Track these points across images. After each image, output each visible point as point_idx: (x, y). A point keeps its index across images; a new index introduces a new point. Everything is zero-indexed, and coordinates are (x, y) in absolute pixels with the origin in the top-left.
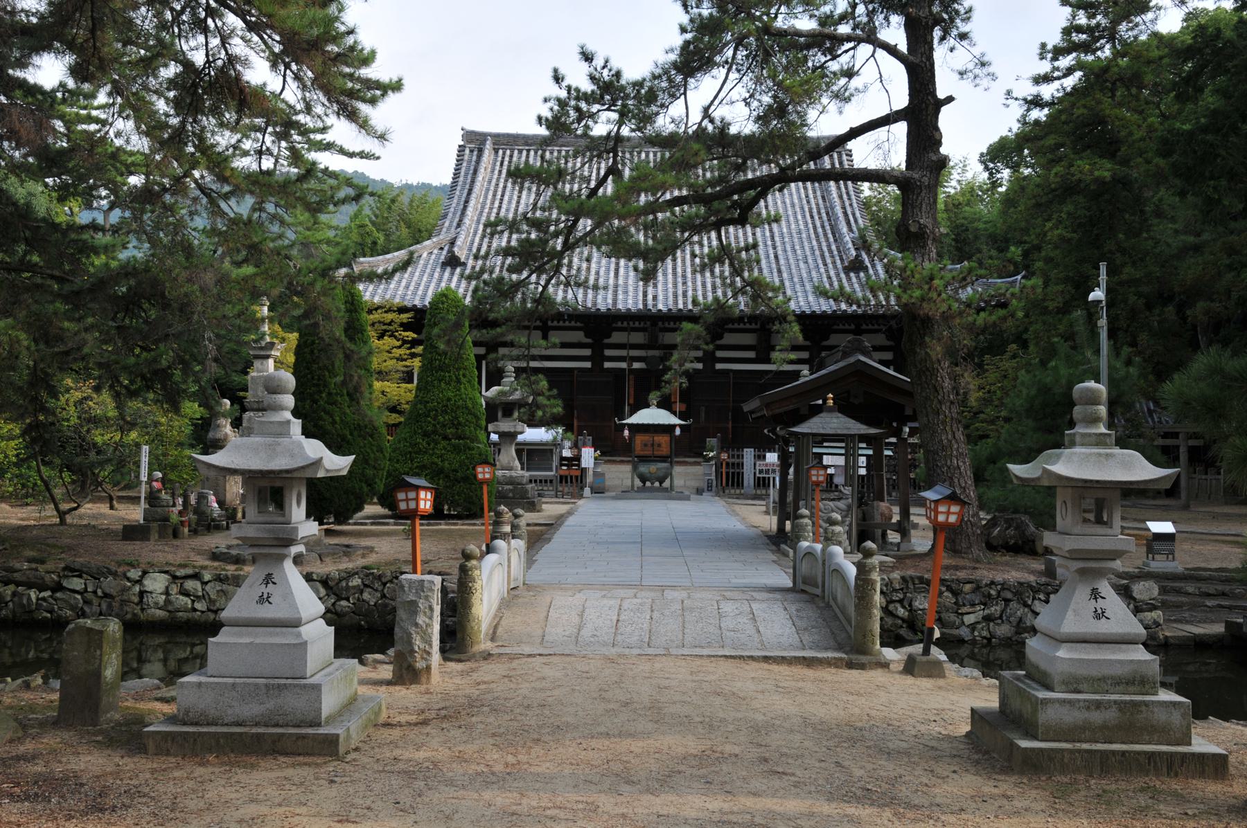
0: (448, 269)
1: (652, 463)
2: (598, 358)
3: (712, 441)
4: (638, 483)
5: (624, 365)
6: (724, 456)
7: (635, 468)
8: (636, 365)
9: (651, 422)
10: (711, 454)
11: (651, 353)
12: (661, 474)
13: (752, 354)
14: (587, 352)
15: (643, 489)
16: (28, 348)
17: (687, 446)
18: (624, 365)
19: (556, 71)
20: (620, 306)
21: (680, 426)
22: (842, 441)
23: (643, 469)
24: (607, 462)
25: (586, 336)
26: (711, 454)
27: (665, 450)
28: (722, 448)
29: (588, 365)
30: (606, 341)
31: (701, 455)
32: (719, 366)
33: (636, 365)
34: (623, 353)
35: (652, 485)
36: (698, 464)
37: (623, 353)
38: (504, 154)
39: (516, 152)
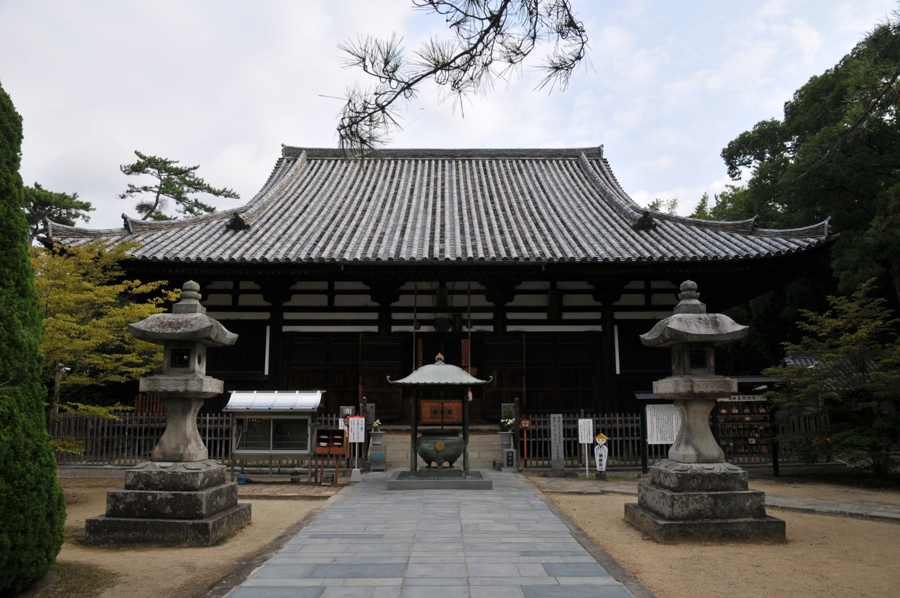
0: (231, 232)
1: (437, 441)
2: (385, 322)
3: (507, 407)
4: (421, 463)
5: (411, 329)
6: (526, 424)
7: (415, 442)
8: (424, 329)
9: (436, 381)
10: (510, 422)
11: (439, 315)
12: (450, 451)
13: (543, 316)
14: (374, 316)
15: (428, 473)
16: (533, 423)
17: (480, 409)
18: (411, 329)
20: (403, 255)
21: (473, 387)
23: (426, 445)
24: (388, 432)
25: (373, 300)
26: (510, 422)
27: (457, 416)
28: (521, 414)
29: (375, 329)
30: (394, 304)
31: (496, 421)
32: (510, 328)
33: (424, 329)
35: (439, 467)
36: (495, 432)
39: (460, 162)
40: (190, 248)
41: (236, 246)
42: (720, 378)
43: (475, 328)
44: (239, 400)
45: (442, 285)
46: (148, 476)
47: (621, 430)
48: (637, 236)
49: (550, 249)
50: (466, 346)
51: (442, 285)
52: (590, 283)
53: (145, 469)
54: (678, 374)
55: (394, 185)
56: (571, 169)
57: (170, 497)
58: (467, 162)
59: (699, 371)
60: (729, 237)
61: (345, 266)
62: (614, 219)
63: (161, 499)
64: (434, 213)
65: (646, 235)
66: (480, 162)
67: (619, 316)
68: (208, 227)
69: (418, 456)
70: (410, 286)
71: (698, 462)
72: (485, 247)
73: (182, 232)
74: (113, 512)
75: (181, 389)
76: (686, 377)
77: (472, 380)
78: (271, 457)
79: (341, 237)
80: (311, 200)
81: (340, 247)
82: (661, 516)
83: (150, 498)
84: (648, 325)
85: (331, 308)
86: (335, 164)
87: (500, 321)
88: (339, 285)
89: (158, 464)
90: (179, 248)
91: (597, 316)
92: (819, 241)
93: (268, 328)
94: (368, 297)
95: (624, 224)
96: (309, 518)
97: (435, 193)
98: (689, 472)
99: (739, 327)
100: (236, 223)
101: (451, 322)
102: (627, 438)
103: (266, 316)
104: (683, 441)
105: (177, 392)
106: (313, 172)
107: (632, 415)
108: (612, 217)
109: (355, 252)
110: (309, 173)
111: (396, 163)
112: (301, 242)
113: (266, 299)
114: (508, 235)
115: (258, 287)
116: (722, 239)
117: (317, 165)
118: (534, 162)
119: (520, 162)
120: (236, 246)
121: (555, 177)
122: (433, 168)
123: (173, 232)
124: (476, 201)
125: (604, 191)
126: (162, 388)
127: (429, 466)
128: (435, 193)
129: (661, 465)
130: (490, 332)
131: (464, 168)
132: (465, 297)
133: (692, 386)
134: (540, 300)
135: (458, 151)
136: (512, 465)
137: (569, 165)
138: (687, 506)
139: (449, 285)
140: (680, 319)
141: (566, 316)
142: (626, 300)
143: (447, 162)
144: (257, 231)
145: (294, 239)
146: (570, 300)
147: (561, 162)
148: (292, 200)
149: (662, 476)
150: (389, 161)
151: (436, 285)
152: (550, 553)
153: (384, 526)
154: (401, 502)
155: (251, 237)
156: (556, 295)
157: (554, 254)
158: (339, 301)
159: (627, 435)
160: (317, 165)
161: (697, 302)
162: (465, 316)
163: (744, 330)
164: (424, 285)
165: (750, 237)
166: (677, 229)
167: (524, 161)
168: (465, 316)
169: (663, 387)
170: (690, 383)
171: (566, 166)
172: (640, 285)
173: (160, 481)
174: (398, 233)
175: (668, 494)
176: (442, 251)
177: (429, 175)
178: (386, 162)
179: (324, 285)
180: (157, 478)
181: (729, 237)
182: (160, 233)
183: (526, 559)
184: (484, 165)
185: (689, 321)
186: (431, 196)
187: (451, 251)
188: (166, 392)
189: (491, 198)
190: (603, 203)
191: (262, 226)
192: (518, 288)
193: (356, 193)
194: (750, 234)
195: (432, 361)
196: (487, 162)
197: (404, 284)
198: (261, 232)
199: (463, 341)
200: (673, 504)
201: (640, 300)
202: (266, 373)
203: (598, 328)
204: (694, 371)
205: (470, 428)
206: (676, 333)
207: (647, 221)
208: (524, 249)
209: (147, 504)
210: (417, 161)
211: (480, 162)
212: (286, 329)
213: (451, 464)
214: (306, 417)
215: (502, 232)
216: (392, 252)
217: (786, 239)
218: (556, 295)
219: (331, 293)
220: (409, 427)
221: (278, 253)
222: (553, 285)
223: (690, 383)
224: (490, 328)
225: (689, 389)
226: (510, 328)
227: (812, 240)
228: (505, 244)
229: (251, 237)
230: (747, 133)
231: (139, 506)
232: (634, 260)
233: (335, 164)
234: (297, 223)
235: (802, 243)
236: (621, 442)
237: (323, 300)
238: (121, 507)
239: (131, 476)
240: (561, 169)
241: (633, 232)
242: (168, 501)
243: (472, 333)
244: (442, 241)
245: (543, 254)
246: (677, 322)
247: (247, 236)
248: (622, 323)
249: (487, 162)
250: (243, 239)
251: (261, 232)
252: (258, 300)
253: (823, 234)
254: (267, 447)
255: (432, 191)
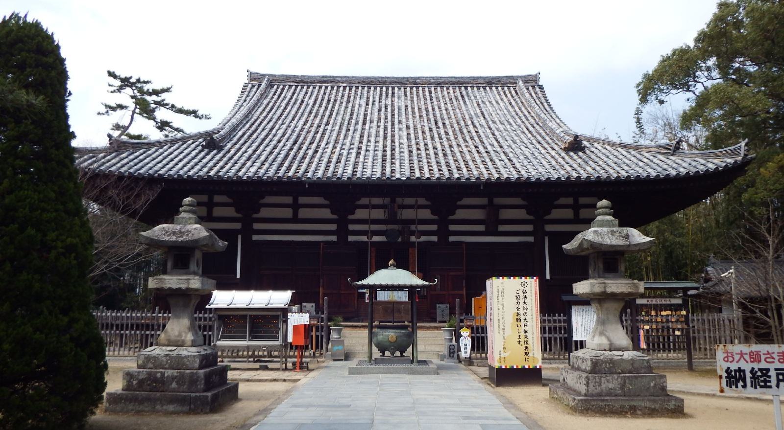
2: (343, 232)
4: (377, 354)
5: (364, 238)
8: (376, 238)
11: (390, 227)
13: (481, 228)
14: (333, 227)
17: (422, 308)
18: (364, 238)
19: (109, 72)
22: (286, 194)
29: (334, 238)
30: (350, 217)
32: (452, 239)
33: (376, 238)
34: (364, 227)
35: (398, 352)
37: (364, 227)
38: (278, 88)
39: (408, 89)
40: (170, 165)
41: (211, 164)
42: (630, 281)
43: (423, 239)
44: (222, 299)
45: (393, 201)
46: (155, 358)
47: (550, 328)
48: (567, 158)
49: (488, 170)
50: (414, 254)
51: (393, 201)
52: (523, 199)
53: (153, 352)
54: (594, 278)
55: (349, 110)
56: (509, 95)
57: (175, 374)
58: (415, 89)
59: (611, 275)
60: (651, 158)
61: (310, 184)
62: (547, 142)
63: (168, 376)
64: (385, 137)
65: (575, 157)
66: (427, 89)
67: (549, 228)
68: (185, 146)
69: (373, 345)
70: (365, 201)
71: (610, 350)
72: (431, 168)
73: (161, 150)
74: (128, 387)
75: (183, 286)
76: (600, 280)
77: (420, 282)
78: (248, 348)
79: (304, 157)
80: (276, 123)
81: (304, 166)
82: (579, 394)
83: (159, 375)
84: (571, 236)
85: (295, 219)
86: (295, 90)
87: (443, 233)
88: (302, 200)
89: (164, 348)
90: (160, 165)
91: (529, 228)
92: (736, 162)
93: (240, 237)
94: (328, 211)
95: (556, 147)
96: (287, 392)
97: (386, 118)
98: (602, 358)
99: (648, 239)
100: (211, 142)
101: (400, 233)
102: (556, 335)
103: (237, 226)
104: (598, 333)
105: (180, 289)
106: (276, 97)
107: (560, 315)
108: (545, 140)
109: (318, 171)
110: (272, 98)
111: (351, 89)
112: (269, 161)
113: (237, 211)
114: (450, 157)
115: (230, 201)
116: (645, 160)
117: (279, 90)
118: (475, 89)
119: (463, 88)
120: (211, 164)
121: (495, 102)
122: (384, 94)
123: (153, 150)
124: (423, 126)
125: (538, 116)
126: (167, 286)
127: (383, 355)
128: (386, 118)
129: (580, 353)
130: (434, 242)
131: (411, 93)
132: (411, 211)
133: (605, 288)
134: (478, 214)
135: (407, 79)
136: (453, 356)
137: (507, 92)
138: (600, 385)
139: (399, 200)
140: (595, 232)
141: (502, 228)
142: (556, 214)
143: (396, 89)
144: (229, 151)
145: (263, 158)
146: (505, 214)
147: (500, 88)
148: (258, 122)
149: (580, 361)
150: (345, 88)
151: (387, 200)
152: (487, 418)
153: (350, 399)
154: (361, 383)
155: (224, 155)
156: (493, 209)
157: (490, 174)
158: (303, 213)
159: (556, 333)
160: (279, 90)
161: (611, 218)
162: (413, 227)
163: (650, 242)
164: (376, 201)
165: (672, 158)
166: (604, 151)
167: (466, 88)
168: (413, 227)
169: (581, 288)
170: (603, 285)
171: (504, 93)
172: (569, 201)
173: (167, 362)
174: (354, 154)
175: (584, 375)
176: (393, 171)
177: (380, 102)
178: (342, 88)
179: (288, 200)
180: (164, 359)
181: (651, 158)
182: (141, 151)
183: (466, 421)
184: (430, 92)
185: (602, 232)
186: (383, 121)
187: (401, 171)
188: (170, 289)
189: (436, 123)
190: (537, 127)
191: (233, 146)
192: (459, 203)
193: (316, 116)
194: (672, 155)
195: (386, 267)
196: (433, 89)
197: (359, 199)
198: (232, 152)
199: (410, 250)
200: (588, 383)
201: (568, 214)
202: (238, 276)
203: (531, 239)
204: (607, 275)
205: (418, 324)
206: (592, 245)
207: (576, 145)
208: (465, 170)
209: (156, 380)
210: (369, 88)
211: (427, 89)
212: (255, 237)
213: (402, 353)
214: (279, 313)
215: (445, 155)
216: (349, 171)
217: (705, 159)
218: (493, 209)
219: (296, 206)
220: (367, 324)
221: (250, 171)
222: (491, 201)
223: (603, 285)
224: (435, 239)
225: (603, 290)
226: (452, 239)
227: (729, 160)
228: (448, 165)
229: (224, 155)
230: (715, 14)
231: (149, 382)
232: (563, 179)
233: (295, 90)
234: (264, 145)
235: (719, 163)
236: (550, 338)
237: (288, 213)
238: (135, 382)
239: (142, 357)
240: (500, 95)
241: (563, 154)
242: (173, 378)
243: (419, 243)
244: (393, 163)
245: (481, 174)
246: (591, 234)
247: (221, 155)
248: (551, 234)
249: (433, 89)
250: (217, 158)
251: (232, 152)
252: (230, 212)
253: (739, 154)
254: (243, 338)
255: (383, 116)
